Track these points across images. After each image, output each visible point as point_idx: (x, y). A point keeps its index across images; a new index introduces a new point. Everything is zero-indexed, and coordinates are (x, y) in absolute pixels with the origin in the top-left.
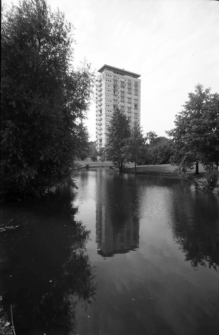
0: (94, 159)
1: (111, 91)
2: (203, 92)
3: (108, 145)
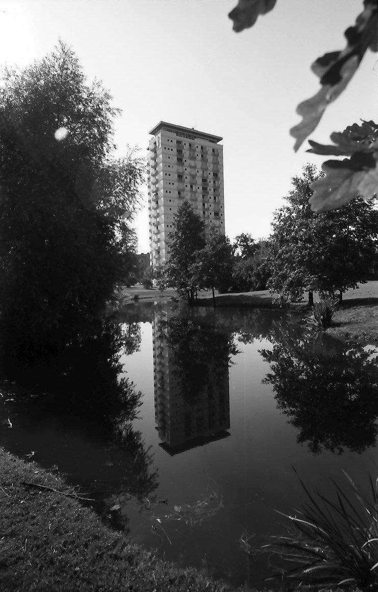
0: (148, 285)
1: (172, 167)
2: (315, 176)
3: (170, 261)
